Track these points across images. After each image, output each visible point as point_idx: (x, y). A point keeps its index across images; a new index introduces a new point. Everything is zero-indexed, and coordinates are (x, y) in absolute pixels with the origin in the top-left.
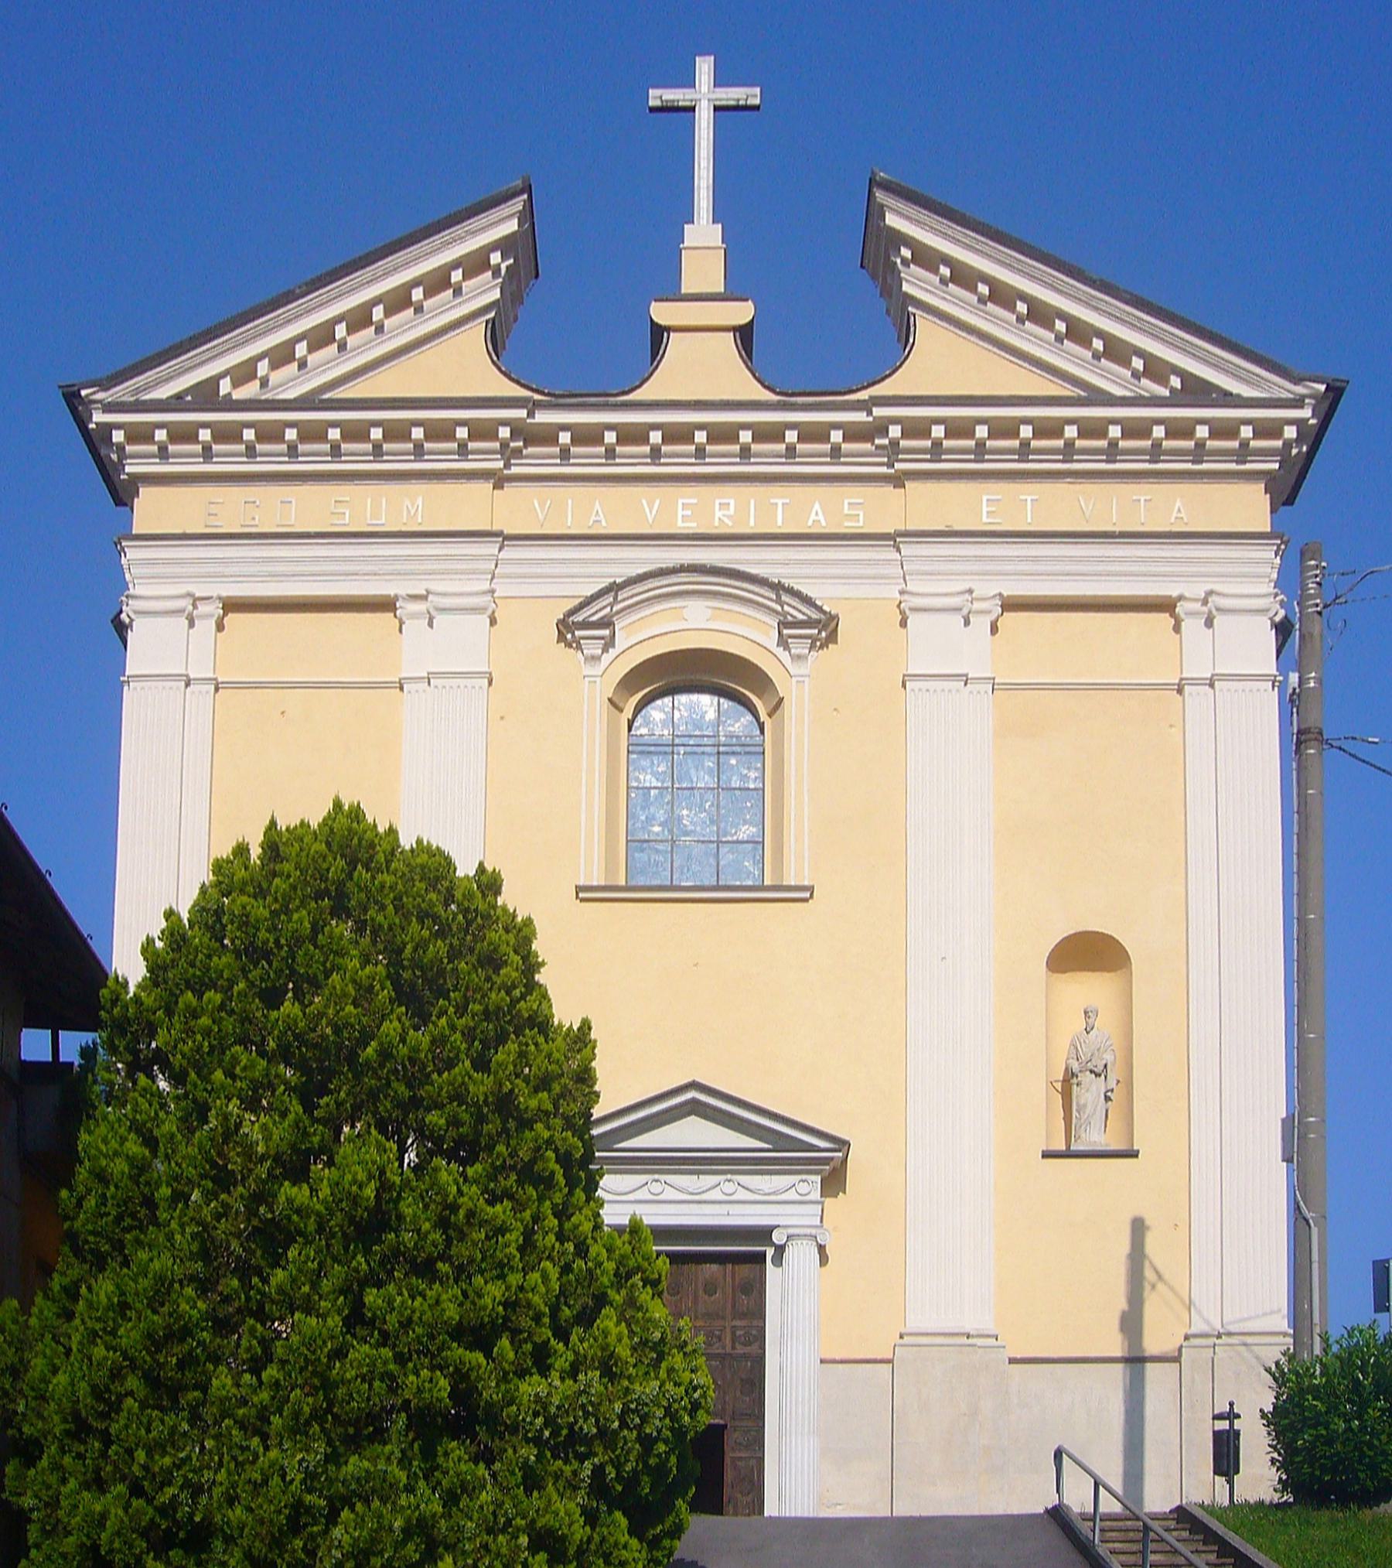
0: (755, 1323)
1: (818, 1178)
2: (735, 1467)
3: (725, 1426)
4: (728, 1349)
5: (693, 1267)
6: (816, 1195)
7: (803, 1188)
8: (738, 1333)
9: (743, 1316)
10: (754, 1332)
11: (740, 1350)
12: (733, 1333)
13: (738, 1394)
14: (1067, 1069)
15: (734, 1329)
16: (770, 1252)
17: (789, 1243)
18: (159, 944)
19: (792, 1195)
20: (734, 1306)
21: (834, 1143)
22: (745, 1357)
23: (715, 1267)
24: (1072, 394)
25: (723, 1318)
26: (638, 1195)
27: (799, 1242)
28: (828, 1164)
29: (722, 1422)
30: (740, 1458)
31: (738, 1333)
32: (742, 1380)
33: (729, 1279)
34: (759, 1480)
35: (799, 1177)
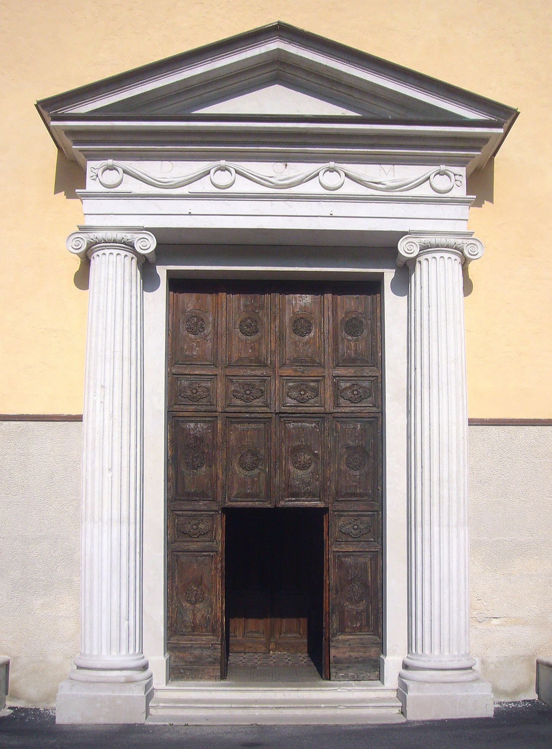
0: (367, 372)
1: (462, 171)
2: (341, 565)
3: (325, 510)
4: (329, 407)
5: (277, 297)
6: (460, 192)
7: (441, 183)
8: (343, 385)
9: (350, 362)
10: (366, 384)
11: (346, 407)
12: (336, 385)
13: (343, 467)
14: (403, 662)
15: (337, 379)
16: (389, 275)
17: (422, 258)
18: (99, 731)
19: (424, 191)
20: (336, 350)
21: (491, 114)
22: (354, 417)
23: (307, 299)
24: (486, 119)
25: (321, 365)
26: (196, 187)
27: (438, 255)
28: (478, 149)
29: (320, 504)
30: (348, 554)
31: (343, 385)
32: (348, 448)
33: (328, 313)
34: (374, 580)
35: (435, 169)
